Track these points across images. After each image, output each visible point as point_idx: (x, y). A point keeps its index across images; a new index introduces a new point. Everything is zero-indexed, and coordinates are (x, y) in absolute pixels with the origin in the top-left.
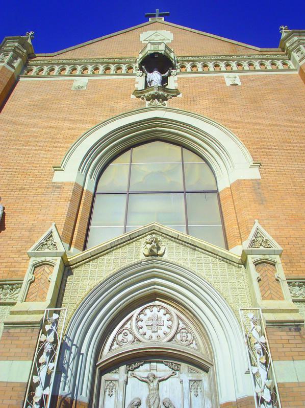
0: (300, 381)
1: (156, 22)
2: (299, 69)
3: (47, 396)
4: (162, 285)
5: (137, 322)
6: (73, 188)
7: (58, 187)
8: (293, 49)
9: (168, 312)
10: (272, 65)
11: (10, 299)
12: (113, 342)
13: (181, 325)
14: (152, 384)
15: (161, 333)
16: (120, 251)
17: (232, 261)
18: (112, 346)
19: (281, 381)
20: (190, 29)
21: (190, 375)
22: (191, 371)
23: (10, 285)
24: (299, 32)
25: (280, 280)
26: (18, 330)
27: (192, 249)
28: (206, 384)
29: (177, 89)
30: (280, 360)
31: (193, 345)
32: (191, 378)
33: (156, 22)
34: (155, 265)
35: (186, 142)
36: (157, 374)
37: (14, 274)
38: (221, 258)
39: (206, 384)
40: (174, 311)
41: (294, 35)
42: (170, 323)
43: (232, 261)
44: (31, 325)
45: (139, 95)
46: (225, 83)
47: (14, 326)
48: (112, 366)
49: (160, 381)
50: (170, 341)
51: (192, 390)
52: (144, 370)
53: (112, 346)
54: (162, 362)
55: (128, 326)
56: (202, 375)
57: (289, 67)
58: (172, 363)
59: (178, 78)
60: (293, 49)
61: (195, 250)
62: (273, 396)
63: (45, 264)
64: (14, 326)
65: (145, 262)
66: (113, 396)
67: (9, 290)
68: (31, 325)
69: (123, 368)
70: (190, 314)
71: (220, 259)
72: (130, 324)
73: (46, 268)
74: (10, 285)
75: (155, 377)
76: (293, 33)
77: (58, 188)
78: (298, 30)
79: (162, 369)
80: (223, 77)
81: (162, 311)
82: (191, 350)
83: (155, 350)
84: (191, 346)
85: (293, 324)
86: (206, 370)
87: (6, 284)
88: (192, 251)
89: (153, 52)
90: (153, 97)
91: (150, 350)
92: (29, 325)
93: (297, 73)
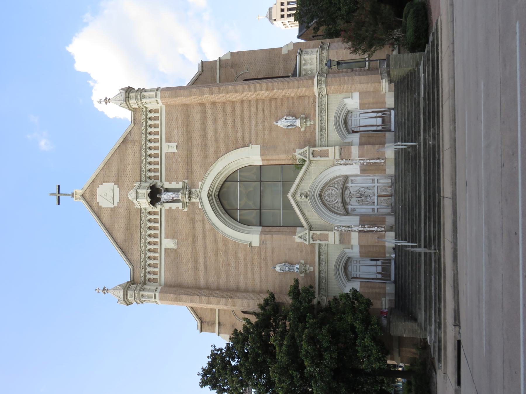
0: (358, 151)
3: (368, 226)
4: (317, 192)
5: (330, 202)
6: (264, 235)
7: (262, 242)
9: (326, 191)
12: (338, 210)
13: (331, 186)
14: (352, 196)
15: (334, 193)
18: (339, 211)
19: (358, 157)
22: (348, 183)
28: (352, 178)
30: (351, 156)
31: (339, 182)
32: (350, 183)
36: (348, 194)
39: (352, 178)
40: (326, 188)
42: (331, 190)
46: (174, 153)
48: (346, 210)
49: (351, 194)
50: (338, 190)
51: (354, 182)
52: (348, 200)
53: (339, 211)
54: (344, 193)
55: (331, 205)
56: (350, 179)
59: (165, 182)
62: (362, 160)
66: (356, 209)
69: (347, 207)
72: (331, 205)
73: (314, 236)
75: (350, 195)
77: (263, 242)
79: (347, 193)
80: (166, 154)
81: (326, 193)
82: (341, 183)
84: (339, 182)
86: (348, 177)
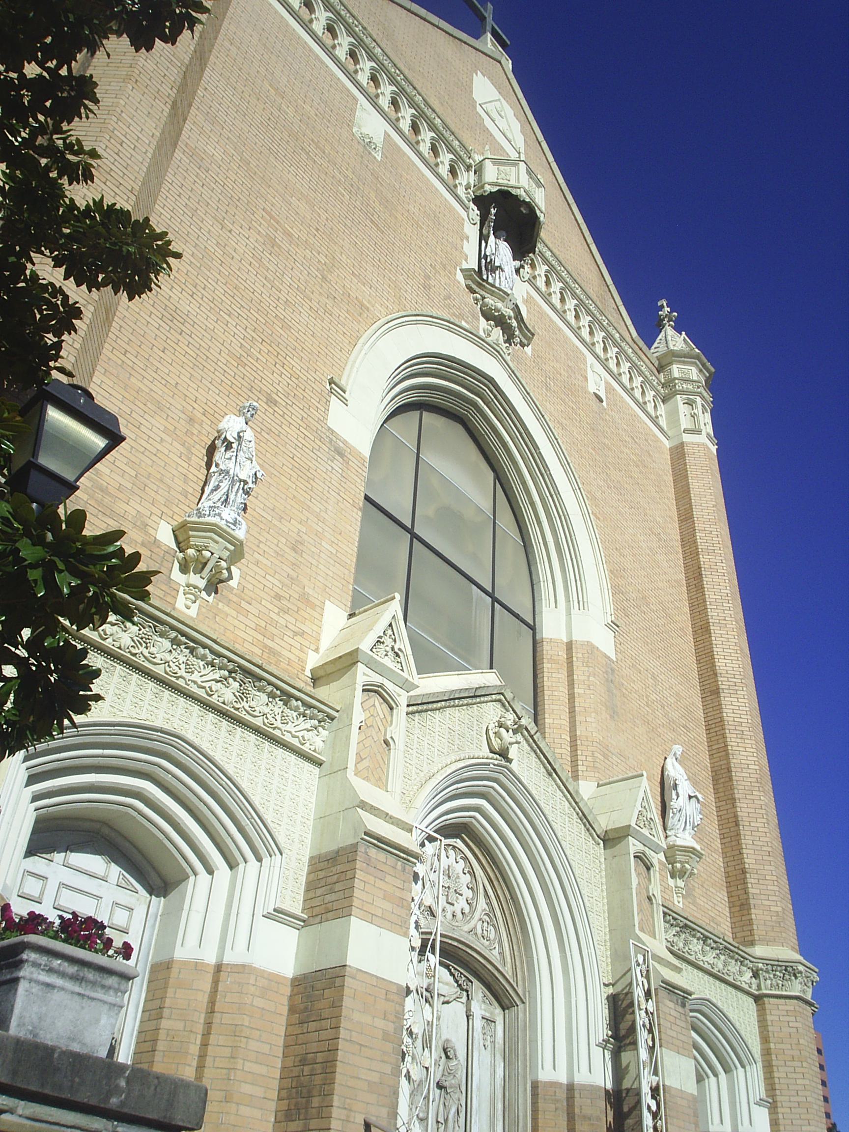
1: (500, 62)
2: (675, 442)
8: (683, 392)
10: (372, 79)
11: (293, 736)
16: (455, 712)
17: (593, 828)
20: (551, 159)
21: (483, 1006)
23: (304, 704)
24: (703, 365)
25: (654, 901)
26: (382, 856)
27: (547, 770)
29: (533, 335)
33: (500, 62)
34: (502, 777)
35: (512, 476)
37: (273, 660)
38: (581, 814)
41: (695, 363)
43: (593, 828)
44: (405, 856)
45: (474, 286)
47: (379, 844)
57: (311, 21)
58: (461, 973)
60: (683, 392)
61: (550, 775)
63: (375, 691)
64: (379, 844)
65: (494, 765)
67: (202, 663)
68: (405, 856)
70: (506, 892)
71: (578, 814)
74: (304, 704)
76: (697, 357)
78: (705, 360)
83: (456, 944)
85: (682, 994)
87: (205, 647)
88: (545, 774)
89: (528, 200)
90: (500, 320)
91: (450, 942)
92: (402, 855)
93: (667, 444)
